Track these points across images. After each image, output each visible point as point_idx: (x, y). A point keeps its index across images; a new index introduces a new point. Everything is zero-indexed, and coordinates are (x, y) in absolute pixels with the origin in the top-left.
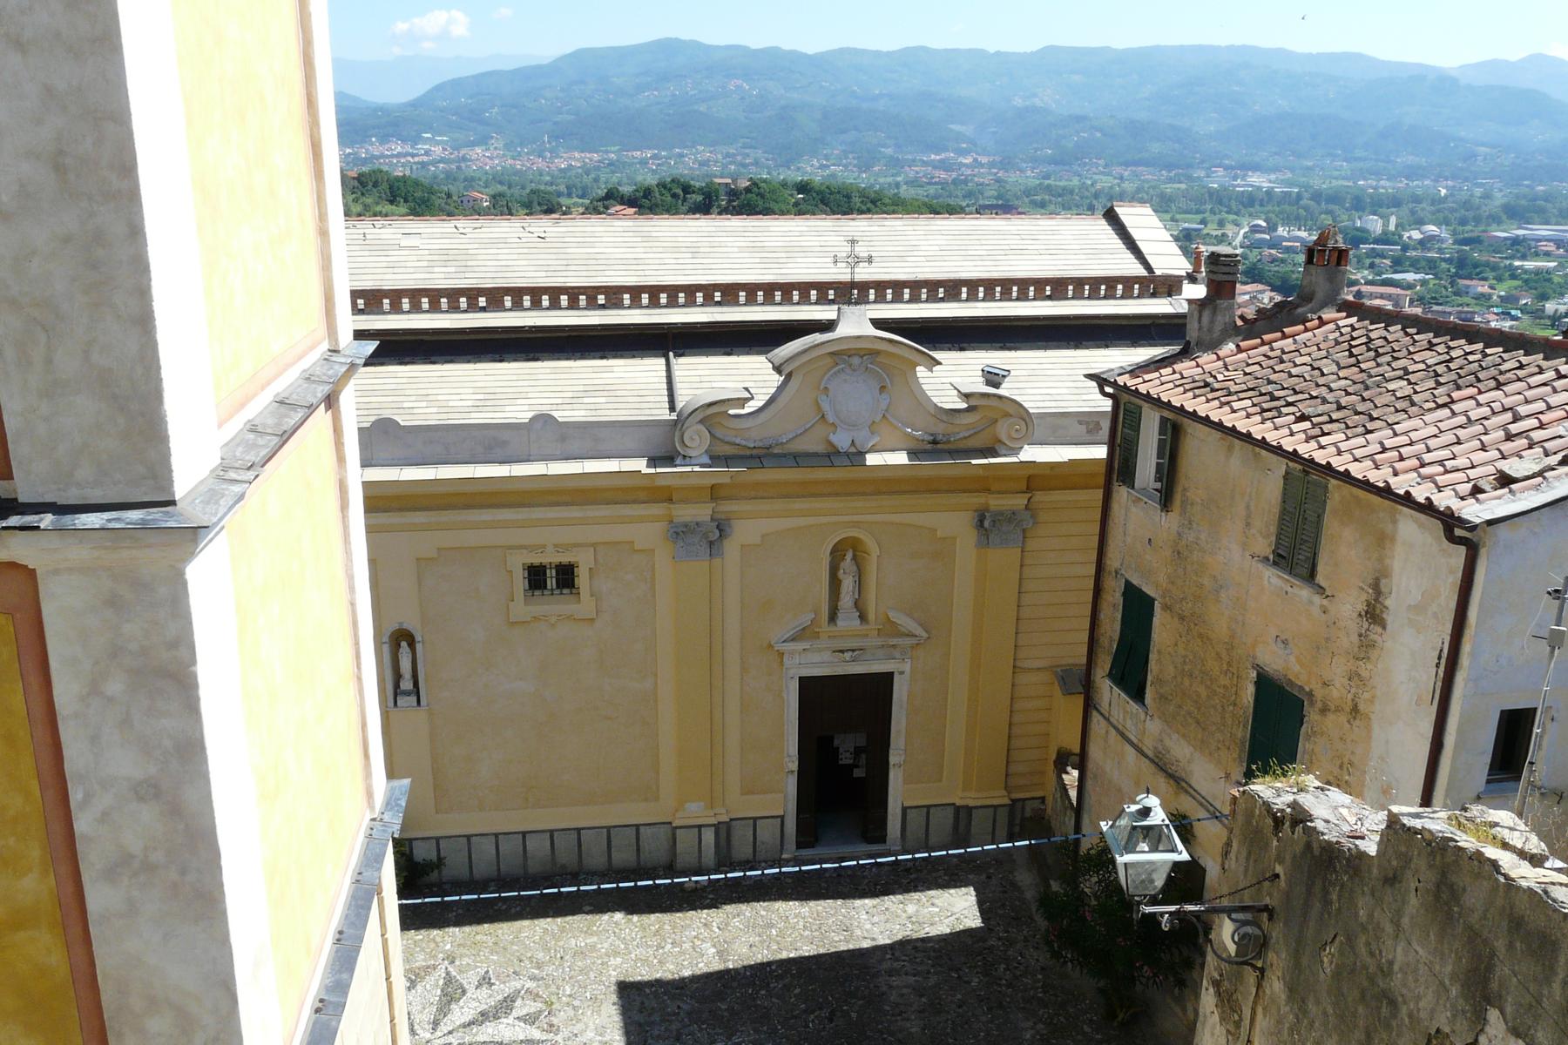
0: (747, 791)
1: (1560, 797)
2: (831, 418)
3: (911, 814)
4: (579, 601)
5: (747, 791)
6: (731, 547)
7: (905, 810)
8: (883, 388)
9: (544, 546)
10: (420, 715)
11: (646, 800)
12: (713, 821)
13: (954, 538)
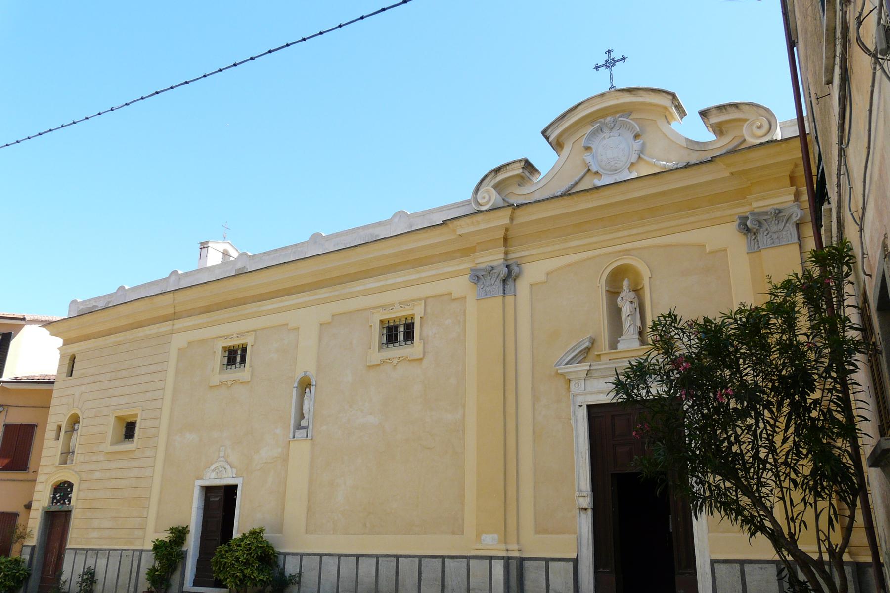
0: (540, 530)
1: (468, 590)
2: (594, 169)
3: (720, 569)
4: (382, 321)
5: (540, 530)
6: (523, 286)
7: (713, 562)
8: (636, 137)
9: (393, 305)
10: (306, 445)
11: (453, 533)
12: (503, 554)
13: (725, 250)
